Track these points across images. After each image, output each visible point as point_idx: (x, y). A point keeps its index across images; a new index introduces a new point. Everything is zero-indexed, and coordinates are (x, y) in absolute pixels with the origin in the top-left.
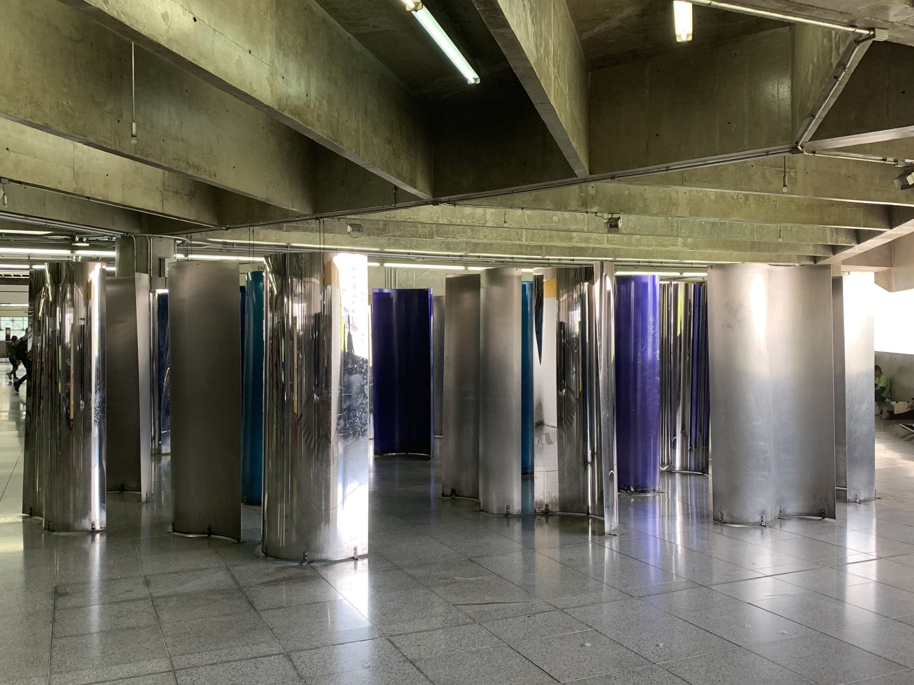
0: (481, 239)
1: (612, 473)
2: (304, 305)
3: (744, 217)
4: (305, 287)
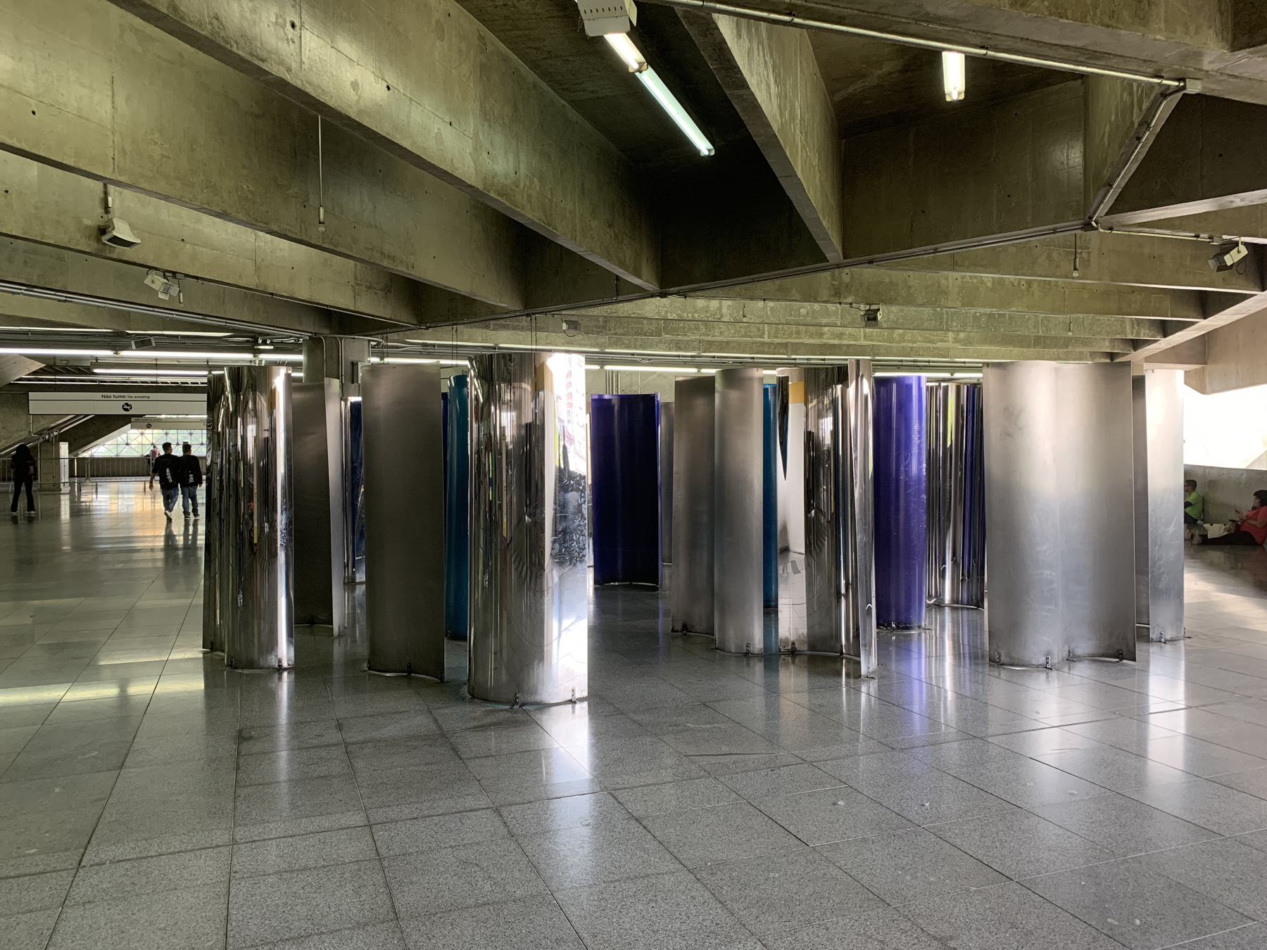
0: (715, 336)
1: (869, 607)
2: (514, 414)
3: (1027, 307)
4: (514, 393)
